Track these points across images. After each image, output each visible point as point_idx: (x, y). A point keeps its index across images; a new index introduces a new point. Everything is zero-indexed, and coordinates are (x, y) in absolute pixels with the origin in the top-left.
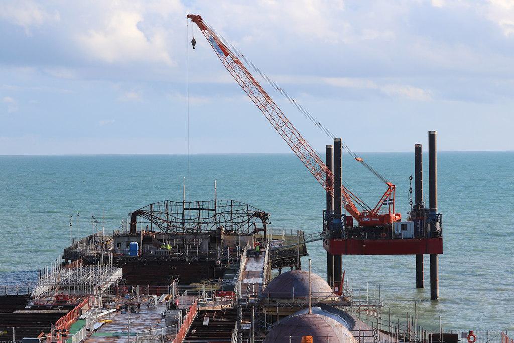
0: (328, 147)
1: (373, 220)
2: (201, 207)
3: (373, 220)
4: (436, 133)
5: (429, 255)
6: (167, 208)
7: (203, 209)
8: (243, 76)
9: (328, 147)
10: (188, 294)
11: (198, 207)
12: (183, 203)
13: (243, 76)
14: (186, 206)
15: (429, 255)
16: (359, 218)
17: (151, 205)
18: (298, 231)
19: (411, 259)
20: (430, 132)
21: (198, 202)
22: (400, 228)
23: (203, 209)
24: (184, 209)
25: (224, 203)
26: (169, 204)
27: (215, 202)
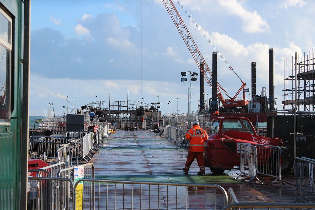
0: (202, 64)
1: (233, 103)
2: (120, 105)
3: (233, 103)
4: (273, 50)
5: (266, 123)
6: (100, 105)
7: (121, 106)
8: (174, 15)
9: (202, 64)
10: (282, 195)
11: (118, 105)
12: (110, 102)
13: (174, 15)
14: (111, 104)
15: (266, 123)
16: (224, 102)
17: (91, 103)
18: (127, 131)
19: (266, 126)
20: (270, 49)
21: (118, 102)
22: (252, 106)
23: (121, 106)
24: (110, 106)
25: (133, 103)
26: (101, 103)
27: (128, 102)
